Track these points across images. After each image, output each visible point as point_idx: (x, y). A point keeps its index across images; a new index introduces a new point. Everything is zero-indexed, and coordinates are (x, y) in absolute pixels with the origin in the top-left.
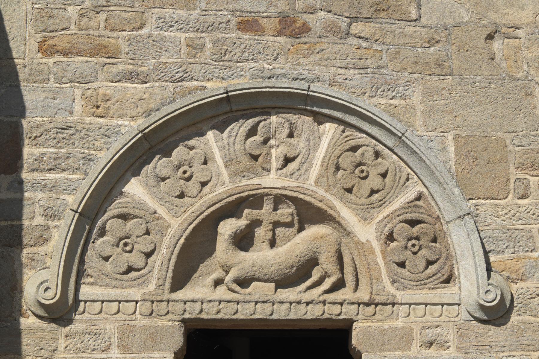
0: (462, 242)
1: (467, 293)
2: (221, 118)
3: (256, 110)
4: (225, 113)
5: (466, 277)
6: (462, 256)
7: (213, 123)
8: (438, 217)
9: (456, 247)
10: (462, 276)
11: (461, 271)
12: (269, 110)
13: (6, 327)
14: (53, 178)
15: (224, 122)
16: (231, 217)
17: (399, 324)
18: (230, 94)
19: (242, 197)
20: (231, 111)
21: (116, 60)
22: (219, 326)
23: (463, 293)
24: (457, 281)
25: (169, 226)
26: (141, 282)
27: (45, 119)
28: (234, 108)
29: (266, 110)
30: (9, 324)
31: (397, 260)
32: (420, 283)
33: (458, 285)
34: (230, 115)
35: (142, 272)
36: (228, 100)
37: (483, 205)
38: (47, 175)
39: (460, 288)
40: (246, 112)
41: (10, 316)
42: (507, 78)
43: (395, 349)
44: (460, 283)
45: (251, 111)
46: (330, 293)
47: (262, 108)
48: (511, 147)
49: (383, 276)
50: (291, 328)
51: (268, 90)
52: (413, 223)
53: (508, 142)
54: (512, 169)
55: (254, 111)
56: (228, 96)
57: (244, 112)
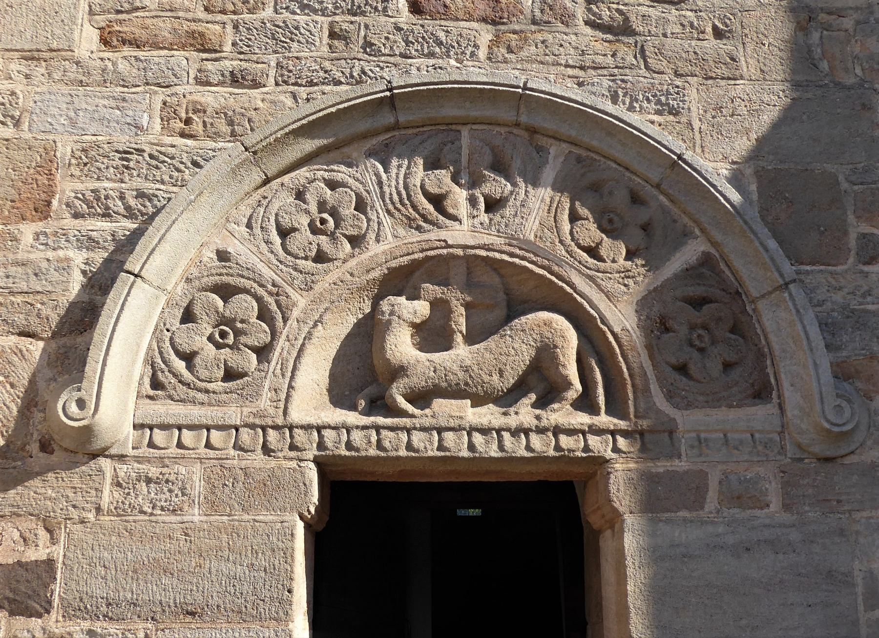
1: (796, 412)
2: (381, 138)
3: (438, 127)
5: (792, 385)
7: (368, 146)
9: (772, 338)
13: (15, 468)
14: (107, 228)
15: (387, 145)
17: (680, 465)
19: (415, 260)
20: (396, 126)
21: (218, 55)
22: (312, 550)
24: (774, 394)
25: (294, 304)
27: (100, 138)
29: (454, 127)
30: (19, 463)
31: (673, 361)
32: (714, 401)
34: (396, 133)
35: (261, 291)
37: (807, 273)
38: (99, 224)
39: (781, 407)
40: (421, 129)
41: (23, 449)
42: (832, 85)
46: (704, 299)
47: (447, 124)
48: (845, 185)
49: (652, 386)
52: (698, 303)
53: (841, 178)
57: (418, 130)
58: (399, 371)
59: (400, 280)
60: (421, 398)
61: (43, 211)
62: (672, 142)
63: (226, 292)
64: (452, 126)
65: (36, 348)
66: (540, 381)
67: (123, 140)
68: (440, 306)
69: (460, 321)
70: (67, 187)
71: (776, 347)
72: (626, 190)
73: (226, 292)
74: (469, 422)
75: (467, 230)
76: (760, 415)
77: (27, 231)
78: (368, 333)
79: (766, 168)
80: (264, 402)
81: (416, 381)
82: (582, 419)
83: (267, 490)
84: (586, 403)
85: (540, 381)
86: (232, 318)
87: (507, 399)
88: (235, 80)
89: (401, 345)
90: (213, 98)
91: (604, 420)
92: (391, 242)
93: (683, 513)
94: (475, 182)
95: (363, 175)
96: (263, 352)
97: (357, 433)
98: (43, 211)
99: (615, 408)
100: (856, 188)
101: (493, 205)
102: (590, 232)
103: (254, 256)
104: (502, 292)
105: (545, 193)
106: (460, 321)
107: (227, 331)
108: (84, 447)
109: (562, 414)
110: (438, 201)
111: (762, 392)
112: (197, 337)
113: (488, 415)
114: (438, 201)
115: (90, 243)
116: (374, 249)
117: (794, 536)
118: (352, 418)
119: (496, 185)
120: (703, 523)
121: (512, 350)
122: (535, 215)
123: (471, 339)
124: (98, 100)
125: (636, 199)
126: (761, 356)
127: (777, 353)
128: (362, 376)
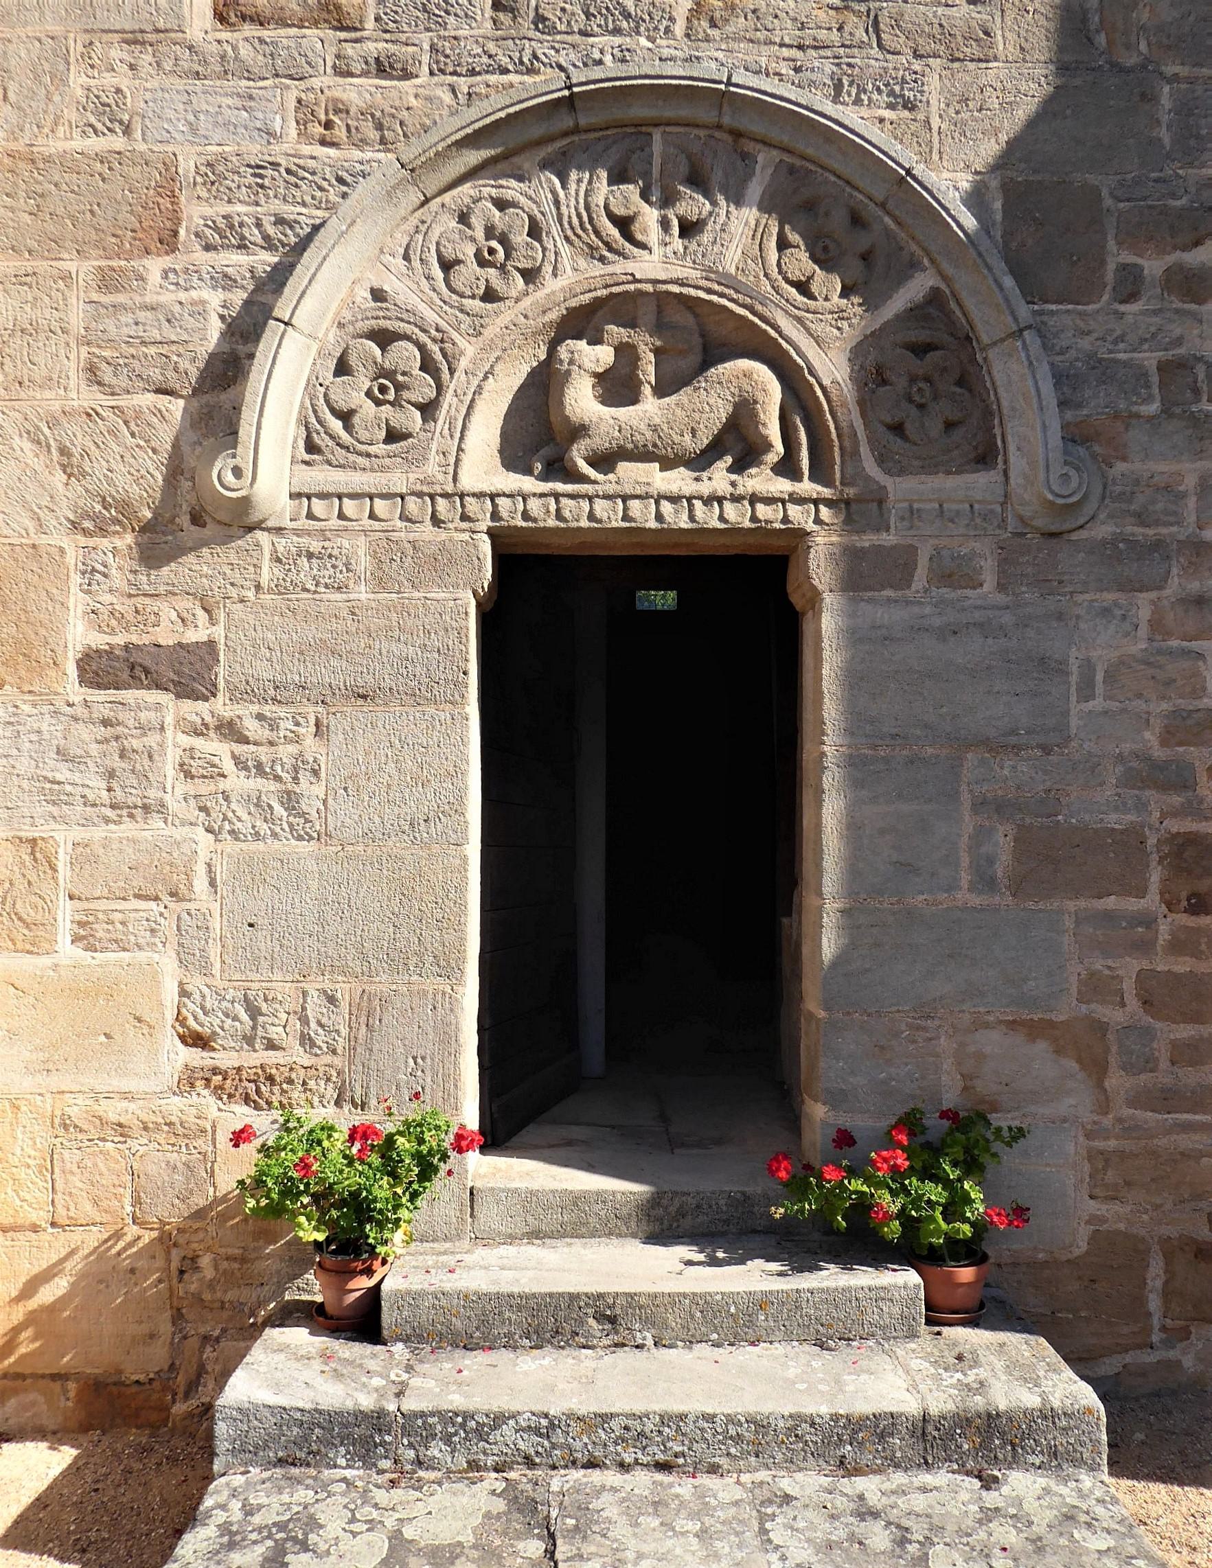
0: (1020, 386)
2: (558, 144)
3: (625, 129)
4: (566, 134)
5: (1019, 449)
6: (1013, 409)
8: (968, 338)
10: (1012, 448)
11: (1009, 438)
12: (650, 129)
15: (564, 154)
16: (179, 1533)
18: (576, 90)
20: (576, 130)
21: (358, 34)
23: (1012, 481)
25: (462, 353)
26: (414, 460)
27: (227, 149)
28: (583, 122)
29: (644, 129)
30: (170, 538)
31: (888, 420)
33: (1000, 466)
34: (576, 138)
36: (570, 103)
37: (1052, 313)
39: (1006, 473)
40: (605, 133)
43: (883, 588)
44: (1006, 462)
45: (615, 131)
50: (683, 552)
51: (647, 82)
53: (1105, 192)
54: (78, 834)
55: (619, 130)
56: (572, 94)
57: (601, 133)
58: (579, 431)
59: (581, 322)
60: (605, 461)
61: (169, 242)
62: (905, 155)
63: (384, 338)
64: (640, 130)
65: (176, 407)
66: (737, 442)
67: (254, 150)
68: (626, 353)
69: (648, 370)
70: (197, 212)
71: (1005, 404)
72: (841, 209)
73: (384, 338)
74: (657, 483)
75: (657, 262)
76: (981, 482)
77: (154, 267)
78: (543, 385)
79: (1024, 184)
80: (432, 467)
81: (598, 442)
82: (783, 486)
83: (436, 565)
84: (788, 467)
85: (737, 442)
86: (394, 368)
87: (700, 461)
88: (382, 68)
89: (581, 399)
90: (358, 92)
91: (807, 487)
92: (571, 277)
93: (889, 593)
94: (667, 200)
95: (537, 192)
96: (428, 410)
97: (534, 501)
98: (169, 242)
99: (820, 473)
100: (1122, 205)
101: (689, 229)
102: (800, 262)
103: (415, 295)
104: (696, 334)
105: (750, 214)
106: (648, 370)
107: (387, 386)
108: (240, 520)
109: (761, 480)
110: (624, 224)
111: (986, 456)
112: (354, 393)
113: (679, 480)
114: (624, 224)
115: (226, 281)
116: (552, 286)
117: (1007, 619)
118: (528, 484)
119: (693, 204)
120: (908, 603)
121: (706, 405)
122: (737, 244)
123: (661, 391)
124: (219, 97)
125: (857, 220)
126: (988, 414)
127: (1005, 411)
128: (538, 435)
